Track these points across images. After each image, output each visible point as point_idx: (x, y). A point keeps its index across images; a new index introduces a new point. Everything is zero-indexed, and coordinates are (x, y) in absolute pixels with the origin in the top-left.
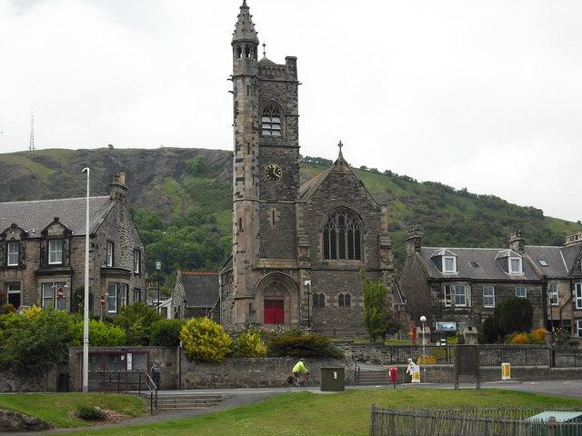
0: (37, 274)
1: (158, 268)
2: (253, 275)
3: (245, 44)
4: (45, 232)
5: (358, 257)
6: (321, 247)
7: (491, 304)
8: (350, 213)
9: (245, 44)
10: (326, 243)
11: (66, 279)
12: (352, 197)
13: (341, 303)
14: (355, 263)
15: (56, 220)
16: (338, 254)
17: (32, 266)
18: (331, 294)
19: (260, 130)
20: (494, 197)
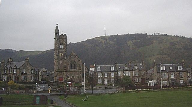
0: (13, 74)
1: (91, 69)
2: (56, 73)
3: (57, 31)
4: (14, 68)
5: (76, 69)
6: (69, 67)
7: (179, 69)
8: (74, 61)
9: (57, 31)
10: (70, 66)
11: (16, 75)
12: (75, 58)
13: (77, 77)
14: (75, 70)
15: (15, 66)
16: (74, 68)
17: (12, 73)
18: (70, 76)
19: (59, 47)
20: (9, 50)
